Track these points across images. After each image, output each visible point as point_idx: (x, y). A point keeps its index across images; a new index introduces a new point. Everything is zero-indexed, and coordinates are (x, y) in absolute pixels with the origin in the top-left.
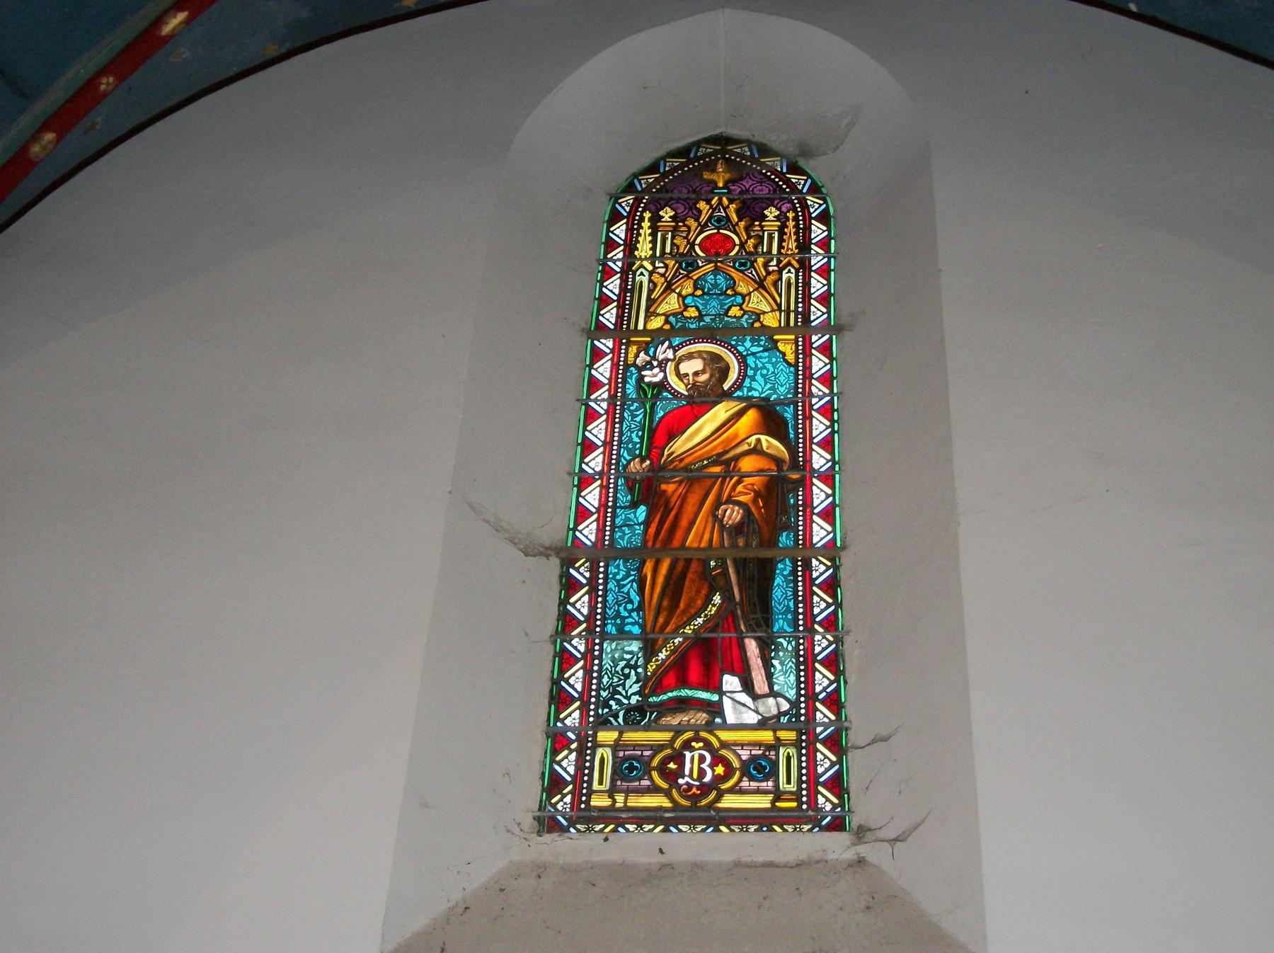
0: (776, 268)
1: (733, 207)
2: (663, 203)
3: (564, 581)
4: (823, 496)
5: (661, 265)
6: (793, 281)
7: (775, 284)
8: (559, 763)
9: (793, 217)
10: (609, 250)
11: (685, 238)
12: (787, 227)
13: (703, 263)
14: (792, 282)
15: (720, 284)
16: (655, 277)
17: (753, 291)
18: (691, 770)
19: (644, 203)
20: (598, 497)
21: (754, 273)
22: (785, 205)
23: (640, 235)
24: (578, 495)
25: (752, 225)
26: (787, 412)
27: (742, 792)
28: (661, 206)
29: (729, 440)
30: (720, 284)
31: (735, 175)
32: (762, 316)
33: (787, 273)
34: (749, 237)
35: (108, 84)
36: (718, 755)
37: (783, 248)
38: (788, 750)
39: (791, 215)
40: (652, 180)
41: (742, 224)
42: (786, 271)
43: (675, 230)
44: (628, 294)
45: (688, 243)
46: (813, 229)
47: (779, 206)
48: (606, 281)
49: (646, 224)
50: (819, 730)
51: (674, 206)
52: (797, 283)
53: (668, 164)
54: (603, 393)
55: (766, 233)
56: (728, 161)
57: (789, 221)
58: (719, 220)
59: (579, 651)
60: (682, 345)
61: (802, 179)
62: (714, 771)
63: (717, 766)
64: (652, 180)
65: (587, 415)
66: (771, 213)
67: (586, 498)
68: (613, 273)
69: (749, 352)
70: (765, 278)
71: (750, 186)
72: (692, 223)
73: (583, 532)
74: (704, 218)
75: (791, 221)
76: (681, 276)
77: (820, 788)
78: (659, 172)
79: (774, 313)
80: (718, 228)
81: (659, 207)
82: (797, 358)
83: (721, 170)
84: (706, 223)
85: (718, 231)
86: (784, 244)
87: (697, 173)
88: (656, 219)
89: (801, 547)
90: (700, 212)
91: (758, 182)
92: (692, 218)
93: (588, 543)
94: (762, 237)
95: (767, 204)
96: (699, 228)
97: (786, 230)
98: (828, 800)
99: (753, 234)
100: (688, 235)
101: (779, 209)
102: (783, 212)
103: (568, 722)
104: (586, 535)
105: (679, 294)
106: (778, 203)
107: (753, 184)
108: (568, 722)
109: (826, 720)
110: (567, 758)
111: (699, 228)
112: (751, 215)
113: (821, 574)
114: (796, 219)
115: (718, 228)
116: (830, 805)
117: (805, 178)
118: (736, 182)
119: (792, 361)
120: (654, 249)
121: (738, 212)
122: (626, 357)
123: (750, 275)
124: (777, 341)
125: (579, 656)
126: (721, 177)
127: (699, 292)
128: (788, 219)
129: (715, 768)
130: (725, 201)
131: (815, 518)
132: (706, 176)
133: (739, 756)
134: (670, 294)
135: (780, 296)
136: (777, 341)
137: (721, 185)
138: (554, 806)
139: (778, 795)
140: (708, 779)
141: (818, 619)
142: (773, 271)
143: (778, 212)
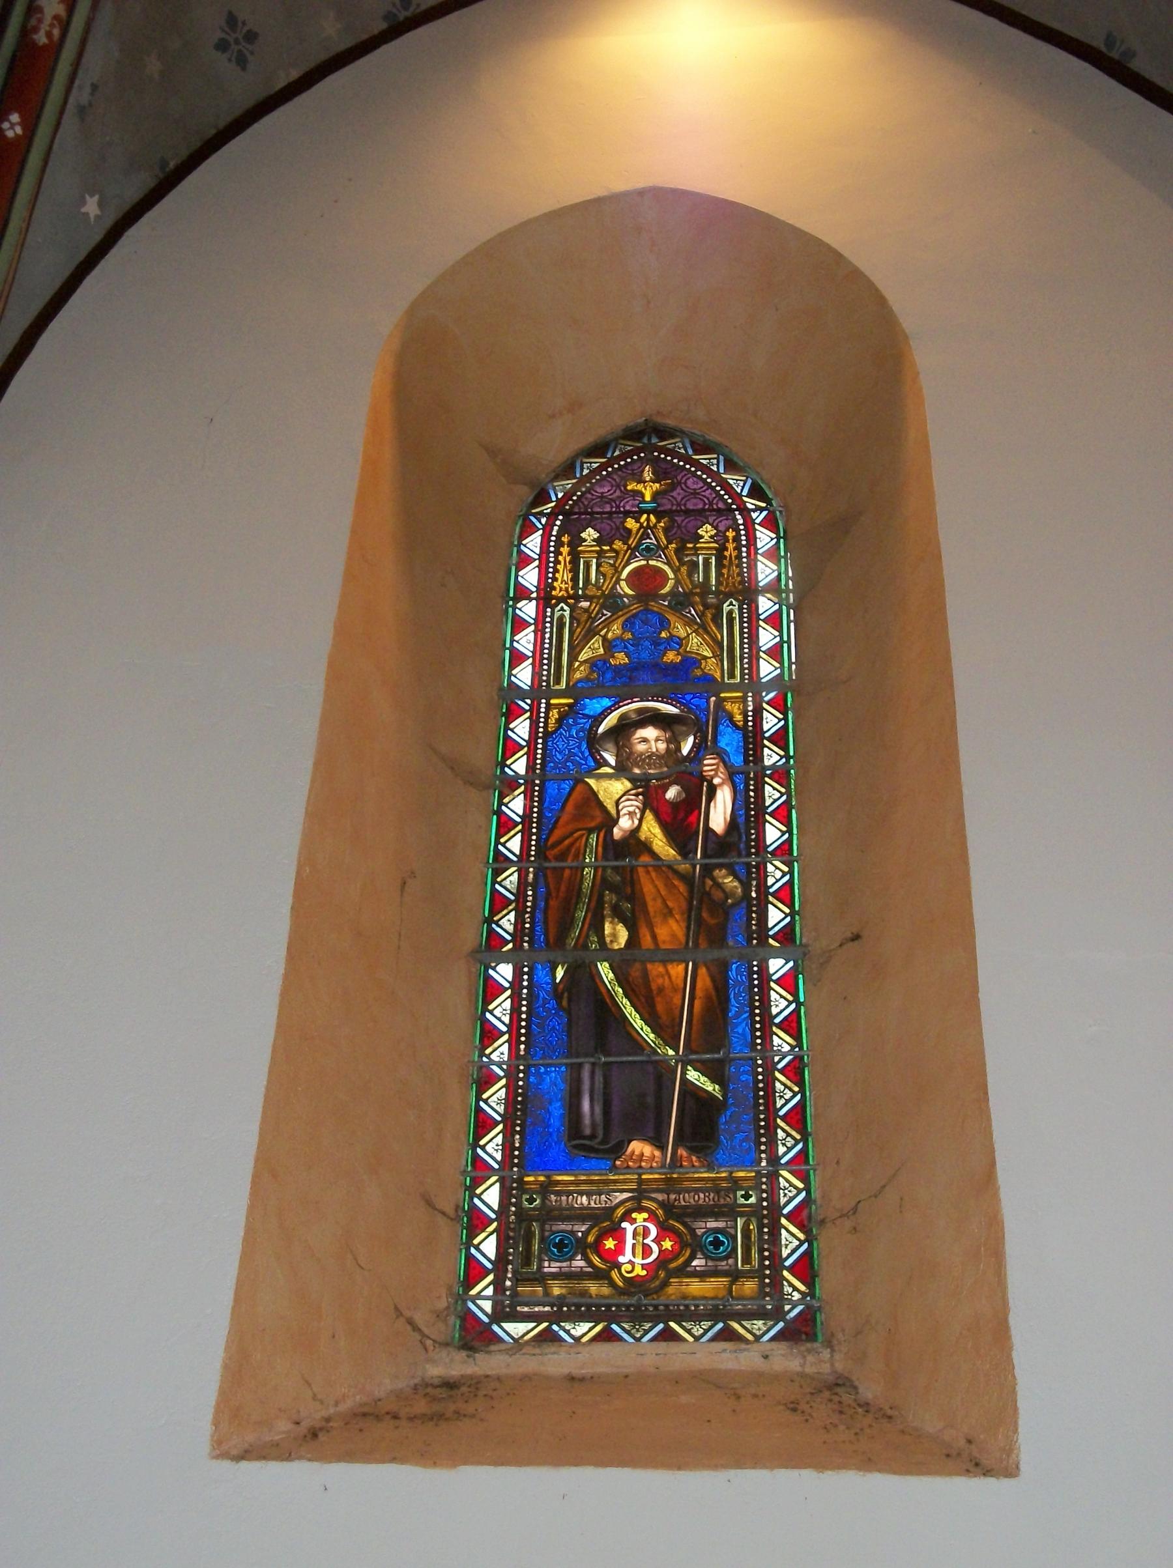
2: (584, 523)
4: (778, 874)
6: (736, 615)
9: (734, 537)
10: (502, 831)
18: (634, 1246)
20: (532, 641)
21: (693, 612)
22: (723, 523)
23: (559, 563)
33: (728, 606)
39: (731, 534)
40: (570, 485)
42: (728, 603)
43: (600, 554)
46: (758, 536)
47: (715, 524)
53: (585, 466)
55: (701, 558)
56: (655, 463)
58: (648, 549)
59: (503, 1023)
61: (741, 480)
62: (660, 1246)
64: (570, 485)
66: (707, 532)
67: (515, 730)
68: (511, 824)
71: (682, 499)
74: (632, 542)
76: (604, 618)
77: (767, 779)
78: (575, 478)
87: (617, 519)
88: (576, 542)
89: (755, 963)
91: (698, 494)
94: (696, 564)
95: (702, 521)
98: (795, 1289)
100: (615, 562)
101: (716, 528)
102: (720, 531)
103: (494, 1057)
105: (604, 638)
106: (714, 520)
108: (494, 1057)
111: (629, 551)
116: (789, 1092)
117: (744, 478)
118: (665, 494)
120: (575, 579)
122: (546, 723)
123: (688, 615)
128: (727, 540)
137: (648, 498)
138: (488, 1056)
143: (715, 531)
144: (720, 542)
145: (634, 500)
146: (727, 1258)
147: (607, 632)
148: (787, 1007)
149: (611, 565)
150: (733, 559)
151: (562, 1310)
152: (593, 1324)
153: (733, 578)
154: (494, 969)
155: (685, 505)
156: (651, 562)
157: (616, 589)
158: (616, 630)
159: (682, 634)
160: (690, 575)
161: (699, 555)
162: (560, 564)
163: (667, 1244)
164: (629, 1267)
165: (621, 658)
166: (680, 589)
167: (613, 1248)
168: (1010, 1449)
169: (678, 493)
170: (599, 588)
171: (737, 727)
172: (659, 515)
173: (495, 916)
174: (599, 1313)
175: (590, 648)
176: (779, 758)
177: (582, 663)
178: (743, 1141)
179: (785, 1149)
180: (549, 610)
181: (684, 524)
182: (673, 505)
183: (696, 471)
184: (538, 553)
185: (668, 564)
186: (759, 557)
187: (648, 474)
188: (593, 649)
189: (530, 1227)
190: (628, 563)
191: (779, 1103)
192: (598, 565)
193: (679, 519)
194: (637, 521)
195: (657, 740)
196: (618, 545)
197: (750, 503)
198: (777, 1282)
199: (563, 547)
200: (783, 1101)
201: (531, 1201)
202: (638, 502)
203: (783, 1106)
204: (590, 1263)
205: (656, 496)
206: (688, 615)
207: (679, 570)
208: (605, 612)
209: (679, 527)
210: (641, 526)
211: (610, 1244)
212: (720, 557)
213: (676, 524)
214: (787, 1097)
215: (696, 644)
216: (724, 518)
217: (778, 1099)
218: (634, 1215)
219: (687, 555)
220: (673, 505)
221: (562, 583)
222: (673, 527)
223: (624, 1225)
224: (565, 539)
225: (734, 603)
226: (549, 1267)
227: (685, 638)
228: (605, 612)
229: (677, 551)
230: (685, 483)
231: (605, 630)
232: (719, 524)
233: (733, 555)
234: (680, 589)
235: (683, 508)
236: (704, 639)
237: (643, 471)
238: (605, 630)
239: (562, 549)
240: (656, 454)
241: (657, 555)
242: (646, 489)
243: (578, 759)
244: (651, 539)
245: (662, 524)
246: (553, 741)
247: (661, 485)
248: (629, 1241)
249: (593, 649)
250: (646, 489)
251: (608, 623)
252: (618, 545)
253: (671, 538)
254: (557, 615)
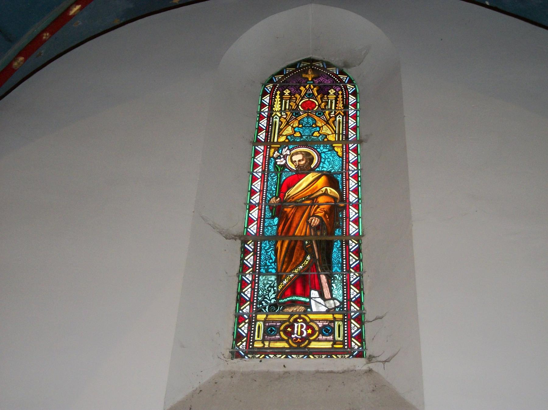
0: (334, 115)
1: (315, 89)
2: (285, 87)
3: (243, 250)
4: (354, 213)
5: (285, 114)
6: (341, 121)
7: (333, 122)
8: (240, 328)
9: (341, 93)
10: (262, 107)
11: (295, 102)
12: (339, 98)
13: (302, 113)
14: (341, 121)
15: (310, 122)
16: (282, 119)
17: (324, 125)
18: (297, 331)
19: (277, 87)
20: (257, 214)
21: (324, 117)
22: (338, 88)
23: (275, 101)
24: (249, 213)
25: (324, 97)
26: (339, 177)
27: (319, 341)
28: (284, 89)
29: (313, 189)
30: (310, 122)
31: (316, 75)
32: (328, 136)
33: (339, 117)
34: (322, 102)
35: (46, 36)
36: (309, 325)
37: (337, 107)
38: (339, 323)
39: (340, 92)
40: (281, 77)
41: (319, 96)
42: (338, 116)
43: (290, 99)
44: (270, 127)
45: (296, 104)
46: (350, 99)
47: (335, 88)
48: (261, 121)
49: (278, 96)
50: (352, 314)
51: (290, 89)
52: (343, 122)
53: (287, 71)
54: (259, 169)
55: (329, 100)
56: (313, 69)
57: (339, 95)
58: (309, 95)
59: (249, 280)
60: (293, 148)
61: (345, 77)
62: (307, 332)
63: (308, 329)
64: (281, 77)
65: (253, 178)
66: (332, 92)
67: (252, 214)
68: (264, 117)
69: (322, 152)
70: (329, 119)
71: (323, 80)
72: (298, 96)
73: (251, 229)
74: (303, 94)
75: (340, 95)
77: (353, 339)
78: (283, 74)
79: (333, 135)
80: (309, 98)
81: (283, 89)
82: (343, 154)
83: (310, 73)
84: (304, 96)
85: (309, 99)
86: (337, 105)
87: (300, 74)
88: (282, 94)
89: (344, 235)
90: (301, 91)
92: (298, 94)
93: (253, 234)
94: (328, 102)
95: (330, 88)
96: (301, 98)
97: (338, 99)
99: (324, 101)
100: (296, 101)
101: (335, 90)
102: (337, 91)
103: (244, 311)
104: (252, 230)
106: (335, 87)
107: (324, 79)
108: (244, 311)
109: (355, 310)
110: (244, 326)
111: (301, 98)
112: (323, 92)
113: (353, 247)
114: (342, 94)
115: (309, 98)
116: (357, 346)
117: (346, 76)
118: (317, 78)
119: (341, 155)
120: (281, 107)
121: (317, 91)
122: (269, 154)
123: (323, 118)
124: (334, 147)
125: (249, 282)
126: (310, 76)
127: (301, 126)
128: (339, 94)
129: (307, 330)
130: (312, 86)
132: (304, 76)
133: (318, 325)
134: (288, 126)
135: (336, 127)
136: (334, 147)
137: (310, 79)
138: (238, 347)
139: (335, 342)
140: (304, 335)
141: (352, 266)
142: (333, 117)
143: (335, 91)
150: (341, 101)
176: (353, 123)
186: (351, 223)
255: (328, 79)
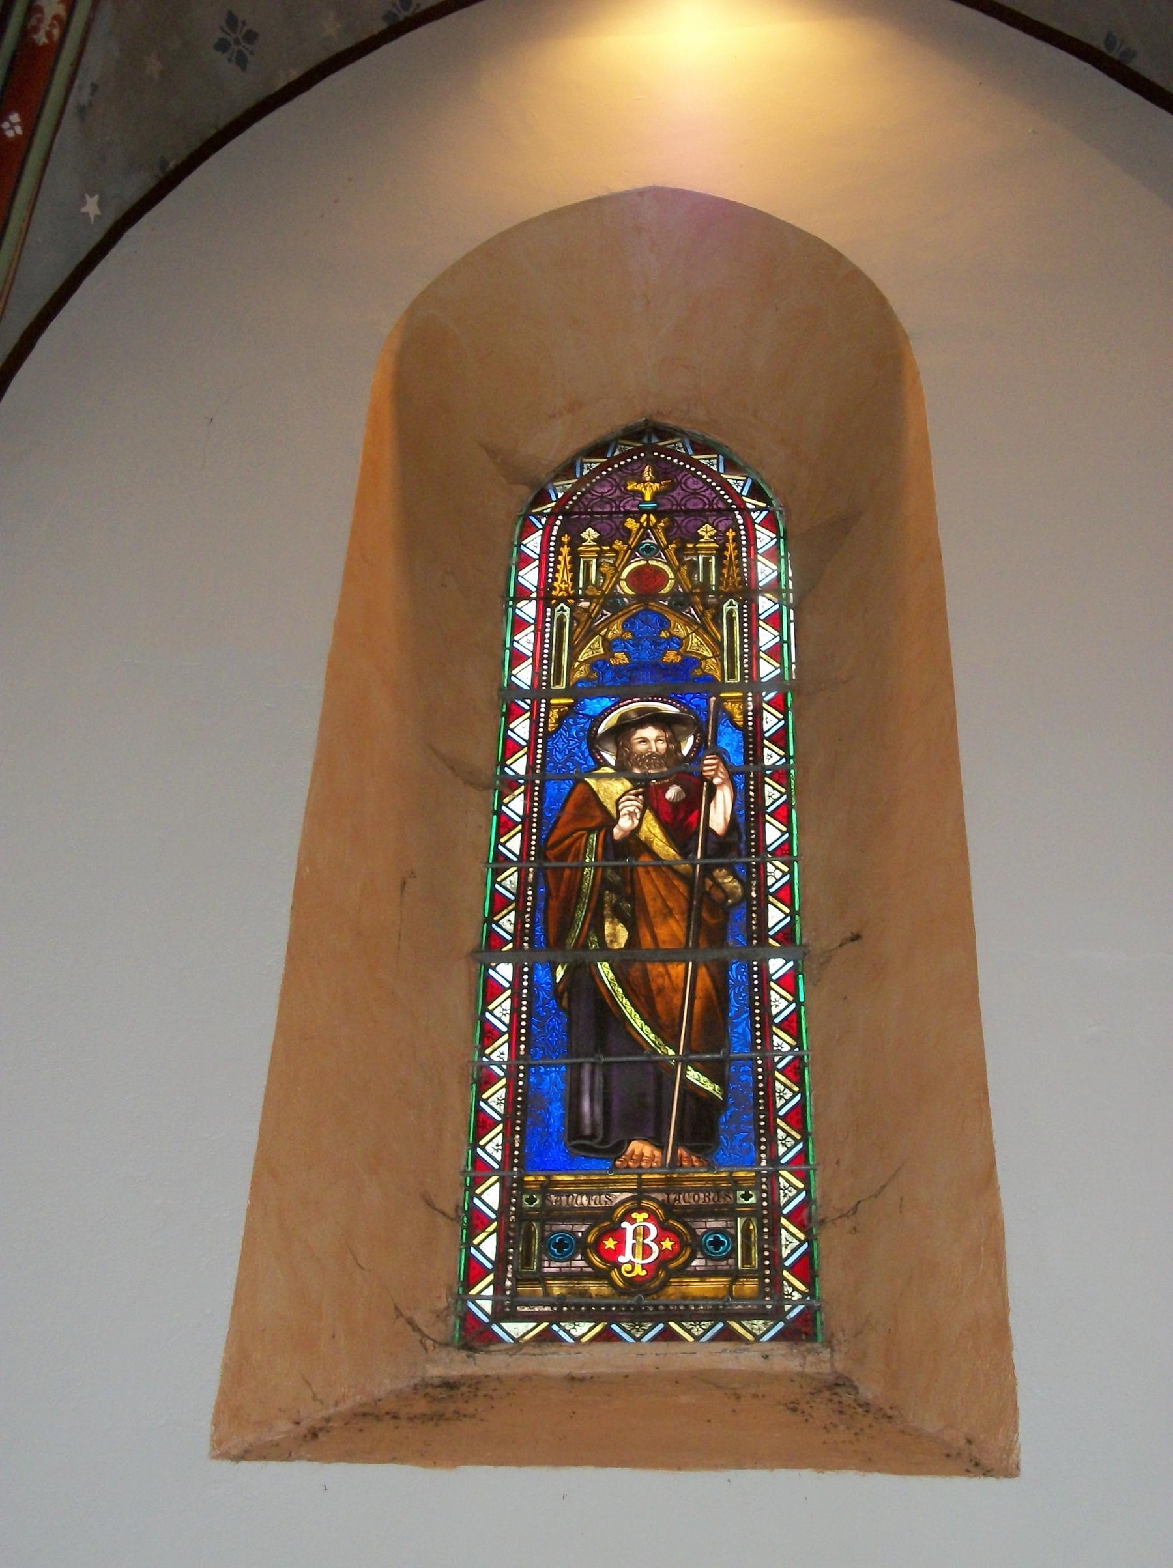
2: (584, 523)
4: (778, 874)
6: (736, 615)
9: (734, 537)
10: (502, 831)
18: (634, 1246)
20: (532, 641)
21: (693, 612)
22: (723, 523)
23: (559, 563)
33: (728, 606)
39: (731, 534)
40: (570, 485)
42: (728, 603)
43: (600, 554)
46: (758, 536)
47: (715, 524)
53: (585, 466)
55: (701, 558)
56: (655, 463)
58: (648, 549)
59: (503, 1023)
61: (741, 480)
62: (660, 1246)
64: (570, 485)
66: (707, 532)
67: (515, 730)
68: (511, 824)
71: (682, 499)
74: (632, 542)
76: (604, 618)
77: (767, 779)
78: (575, 478)
87: (617, 519)
88: (576, 542)
89: (755, 963)
91: (698, 494)
94: (696, 564)
95: (702, 521)
98: (795, 1289)
100: (615, 562)
101: (716, 528)
102: (720, 531)
103: (494, 1057)
105: (604, 638)
106: (714, 520)
108: (494, 1057)
111: (629, 551)
116: (789, 1092)
117: (744, 478)
118: (665, 494)
120: (575, 579)
122: (546, 723)
123: (688, 615)
128: (727, 540)
131: (759, 557)
137: (648, 498)
138: (488, 1056)
143: (715, 531)
144: (720, 542)
145: (634, 500)
146: (727, 1258)
147: (607, 632)
148: (787, 1007)
149: (611, 565)
150: (733, 559)
151: (562, 1310)
152: (593, 1324)
153: (733, 578)
154: (494, 969)
155: (685, 505)
156: (651, 562)
157: (616, 589)
158: (616, 630)
159: (682, 634)
160: (690, 575)
161: (699, 555)
162: (560, 564)
163: (667, 1244)
164: (629, 1267)
165: (621, 658)
166: (680, 589)
167: (613, 1248)
168: (1010, 1449)
169: (678, 493)
170: (599, 588)
171: (737, 727)
172: (659, 515)
173: (495, 916)
174: (599, 1313)
175: (590, 648)
176: (779, 758)
177: (582, 663)
178: (743, 1141)
179: (785, 1149)
180: (549, 610)
181: (684, 524)
182: (673, 505)
183: (696, 471)
184: (538, 553)
185: (668, 564)
187: (648, 474)
188: (593, 649)
189: (530, 1227)
190: (628, 563)
191: (779, 1103)
192: (598, 565)
193: (679, 519)
194: (637, 521)
195: (657, 740)
196: (618, 545)
197: (750, 503)
198: (777, 1282)
199: (563, 547)
200: (783, 1101)
201: (531, 1201)
202: (638, 502)
203: (783, 1106)
204: (590, 1263)
205: (656, 496)
206: (688, 615)
207: (679, 570)
208: (605, 612)
209: (679, 527)
210: (641, 526)
211: (610, 1244)
212: (720, 557)
213: (676, 524)
214: (787, 1097)
215: (696, 644)
216: (724, 518)
217: (778, 1099)
218: (634, 1215)
219: (687, 555)
220: (673, 505)
221: (562, 583)
222: (673, 527)
223: (624, 1225)
224: (565, 539)
225: (734, 603)
226: (549, 1267)
227: (685, 638)
228: (605, 612)
229: (677, 551)
230: (685, 483)
231: (605, 630)
232: (719, 524)
233: (733, 555)
234: (680, 589)
235: (683, 508)
236: (704, 639)
237: (643, 471)
238: (605, 630)
239: (562, 549)
240: (656, 454)
241: (657, 555)
242: (646, 489)
243: (578, 759)
244: (651, 539)
245: (662, 524)
246: (553, 741)
247: (661, 485)
248: (629, 1241)
249: (593, 649)
250: (646, 489)
251: (608, 623)
252: (618, 545)
253: (671, 538)
254: (557, 615)
255: (692, 491)
